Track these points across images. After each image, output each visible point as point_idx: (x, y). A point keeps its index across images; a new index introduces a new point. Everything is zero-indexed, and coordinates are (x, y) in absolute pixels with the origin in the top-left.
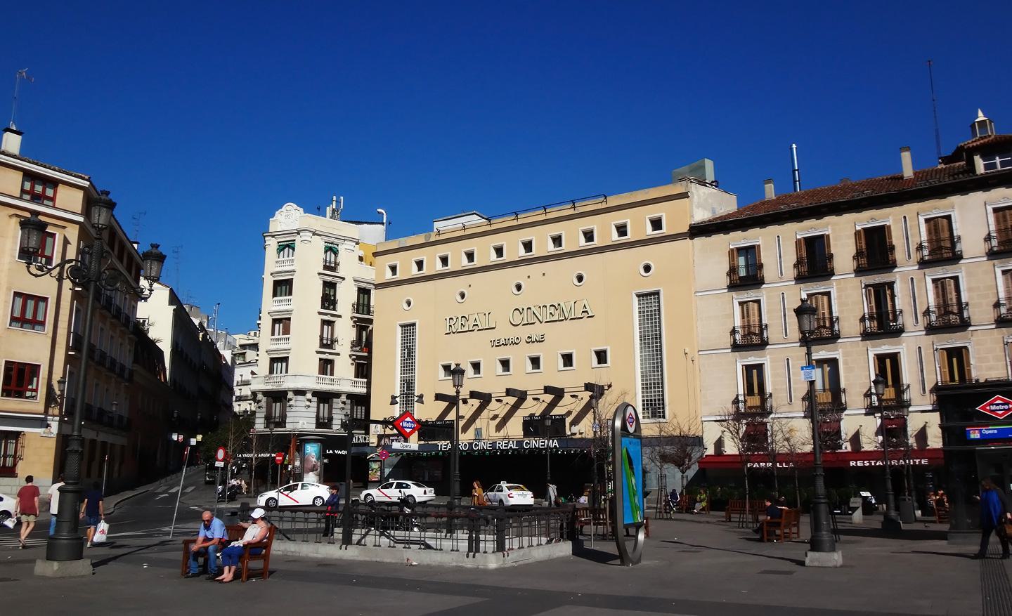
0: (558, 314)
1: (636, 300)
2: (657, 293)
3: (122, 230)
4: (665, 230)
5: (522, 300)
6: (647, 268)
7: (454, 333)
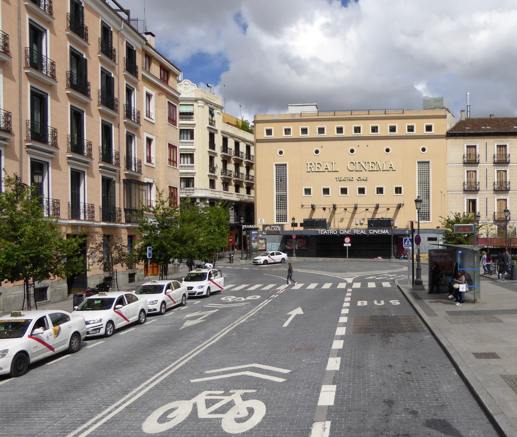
0: (375, 168)
1: (417, 164)
2: (428, 162)
3: (185, 105)
4: (433, 132)
5: (354, 157)
6: (424, 150)
7: (313, 172)
